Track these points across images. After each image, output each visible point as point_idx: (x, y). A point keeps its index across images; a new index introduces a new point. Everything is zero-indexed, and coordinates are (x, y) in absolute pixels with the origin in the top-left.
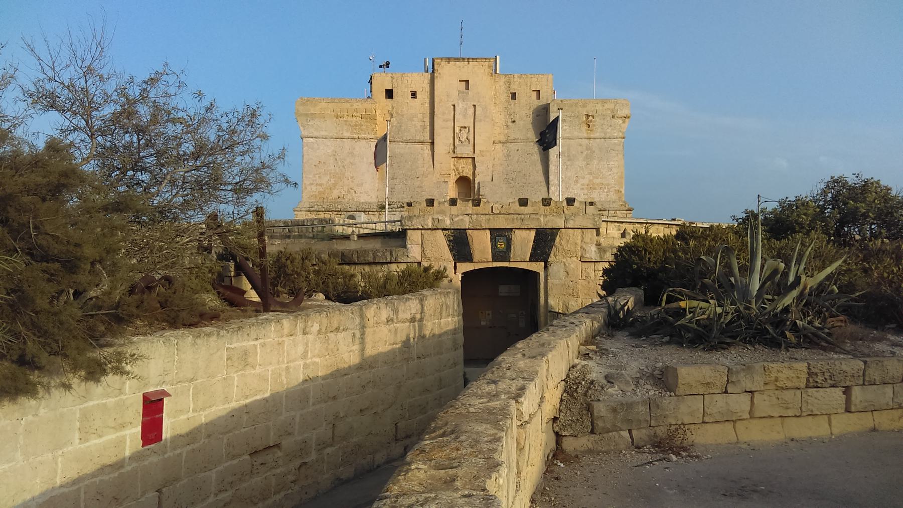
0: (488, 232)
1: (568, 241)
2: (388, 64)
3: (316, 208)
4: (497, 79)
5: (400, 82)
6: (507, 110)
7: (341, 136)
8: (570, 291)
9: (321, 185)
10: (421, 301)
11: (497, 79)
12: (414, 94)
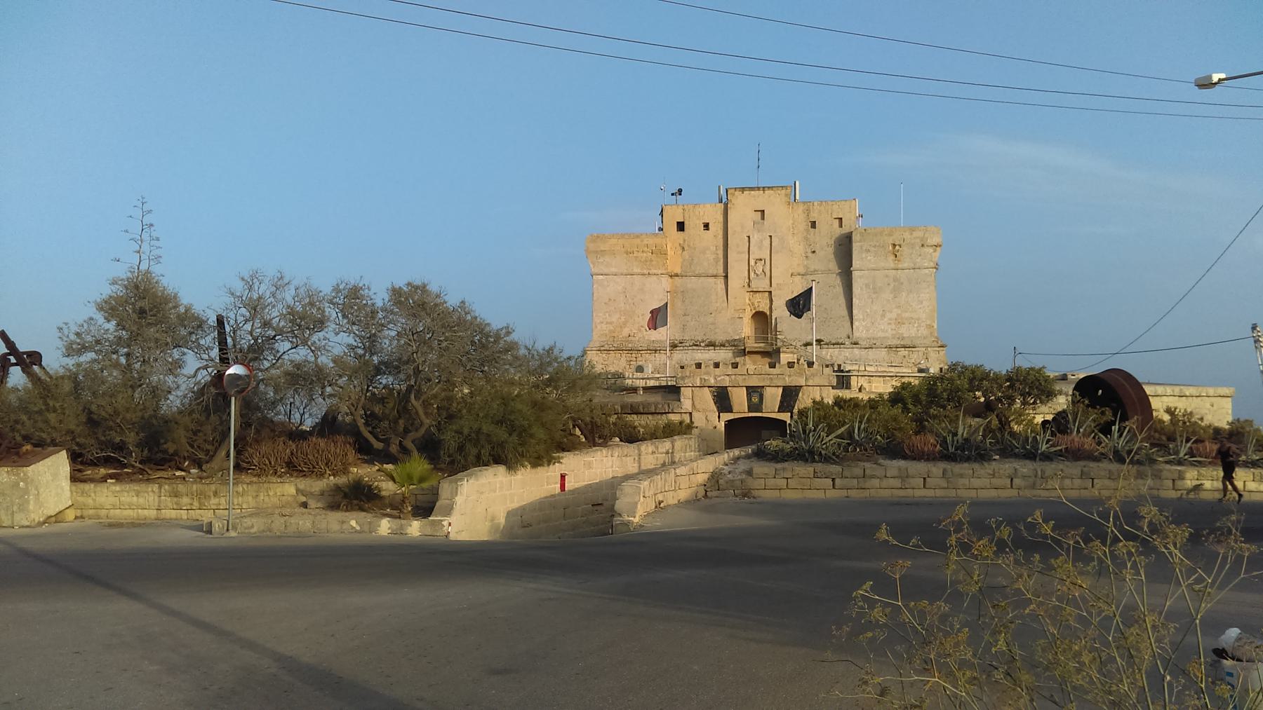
2: (680, 191)
3: (606, 347)
6: (806, 239)
9: (611, 323)
10: (672, 443)
12: (706, 226)
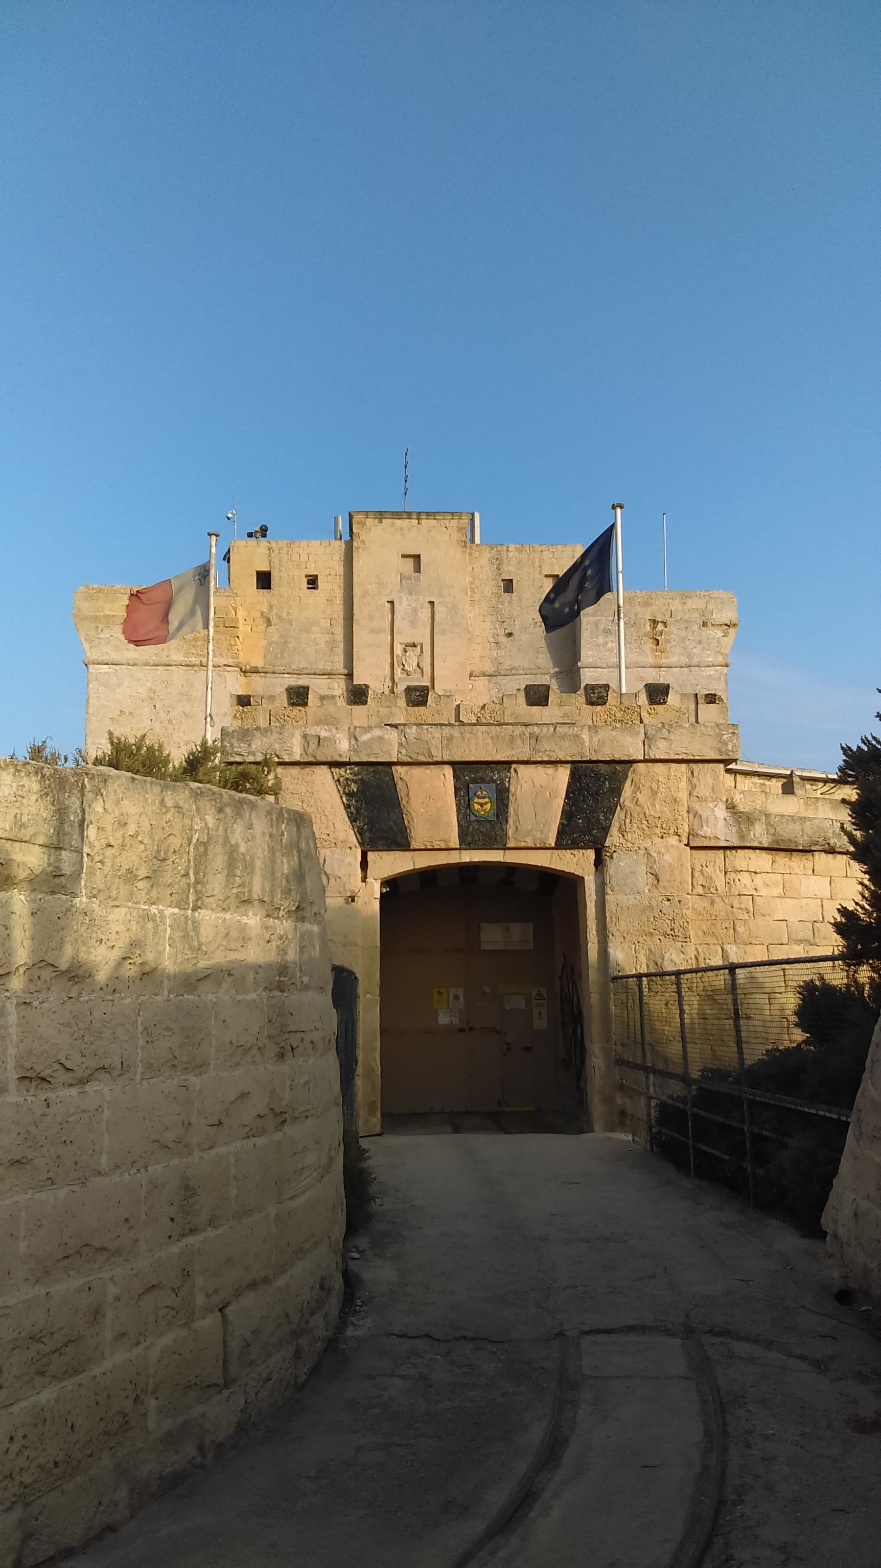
0: (448, 771)
1: (654, 793)
2: (264, 531)
4: (476, 554)
5: (285, 558)
7: (165, 660)
8: (666, 927)
11: (476, 554)
12: (313, 582)
